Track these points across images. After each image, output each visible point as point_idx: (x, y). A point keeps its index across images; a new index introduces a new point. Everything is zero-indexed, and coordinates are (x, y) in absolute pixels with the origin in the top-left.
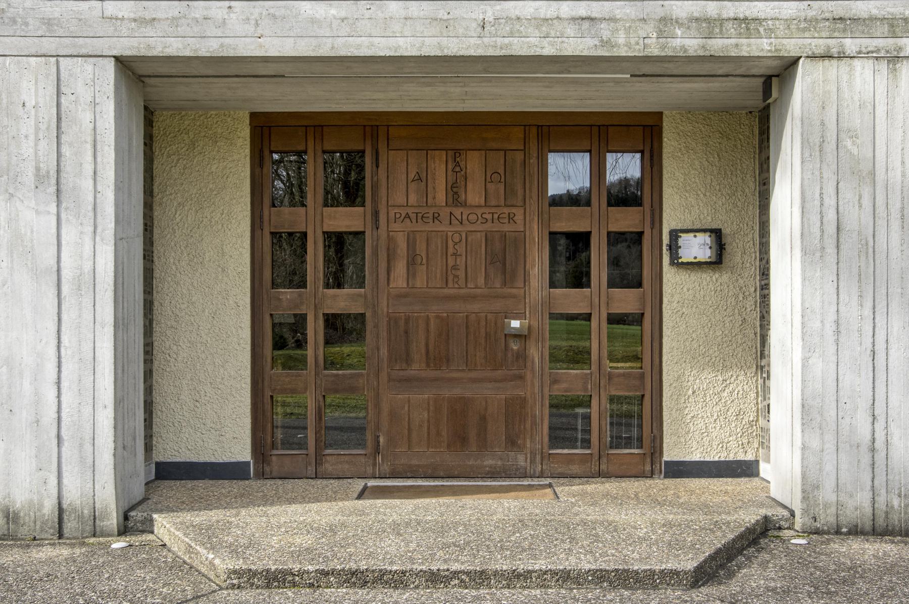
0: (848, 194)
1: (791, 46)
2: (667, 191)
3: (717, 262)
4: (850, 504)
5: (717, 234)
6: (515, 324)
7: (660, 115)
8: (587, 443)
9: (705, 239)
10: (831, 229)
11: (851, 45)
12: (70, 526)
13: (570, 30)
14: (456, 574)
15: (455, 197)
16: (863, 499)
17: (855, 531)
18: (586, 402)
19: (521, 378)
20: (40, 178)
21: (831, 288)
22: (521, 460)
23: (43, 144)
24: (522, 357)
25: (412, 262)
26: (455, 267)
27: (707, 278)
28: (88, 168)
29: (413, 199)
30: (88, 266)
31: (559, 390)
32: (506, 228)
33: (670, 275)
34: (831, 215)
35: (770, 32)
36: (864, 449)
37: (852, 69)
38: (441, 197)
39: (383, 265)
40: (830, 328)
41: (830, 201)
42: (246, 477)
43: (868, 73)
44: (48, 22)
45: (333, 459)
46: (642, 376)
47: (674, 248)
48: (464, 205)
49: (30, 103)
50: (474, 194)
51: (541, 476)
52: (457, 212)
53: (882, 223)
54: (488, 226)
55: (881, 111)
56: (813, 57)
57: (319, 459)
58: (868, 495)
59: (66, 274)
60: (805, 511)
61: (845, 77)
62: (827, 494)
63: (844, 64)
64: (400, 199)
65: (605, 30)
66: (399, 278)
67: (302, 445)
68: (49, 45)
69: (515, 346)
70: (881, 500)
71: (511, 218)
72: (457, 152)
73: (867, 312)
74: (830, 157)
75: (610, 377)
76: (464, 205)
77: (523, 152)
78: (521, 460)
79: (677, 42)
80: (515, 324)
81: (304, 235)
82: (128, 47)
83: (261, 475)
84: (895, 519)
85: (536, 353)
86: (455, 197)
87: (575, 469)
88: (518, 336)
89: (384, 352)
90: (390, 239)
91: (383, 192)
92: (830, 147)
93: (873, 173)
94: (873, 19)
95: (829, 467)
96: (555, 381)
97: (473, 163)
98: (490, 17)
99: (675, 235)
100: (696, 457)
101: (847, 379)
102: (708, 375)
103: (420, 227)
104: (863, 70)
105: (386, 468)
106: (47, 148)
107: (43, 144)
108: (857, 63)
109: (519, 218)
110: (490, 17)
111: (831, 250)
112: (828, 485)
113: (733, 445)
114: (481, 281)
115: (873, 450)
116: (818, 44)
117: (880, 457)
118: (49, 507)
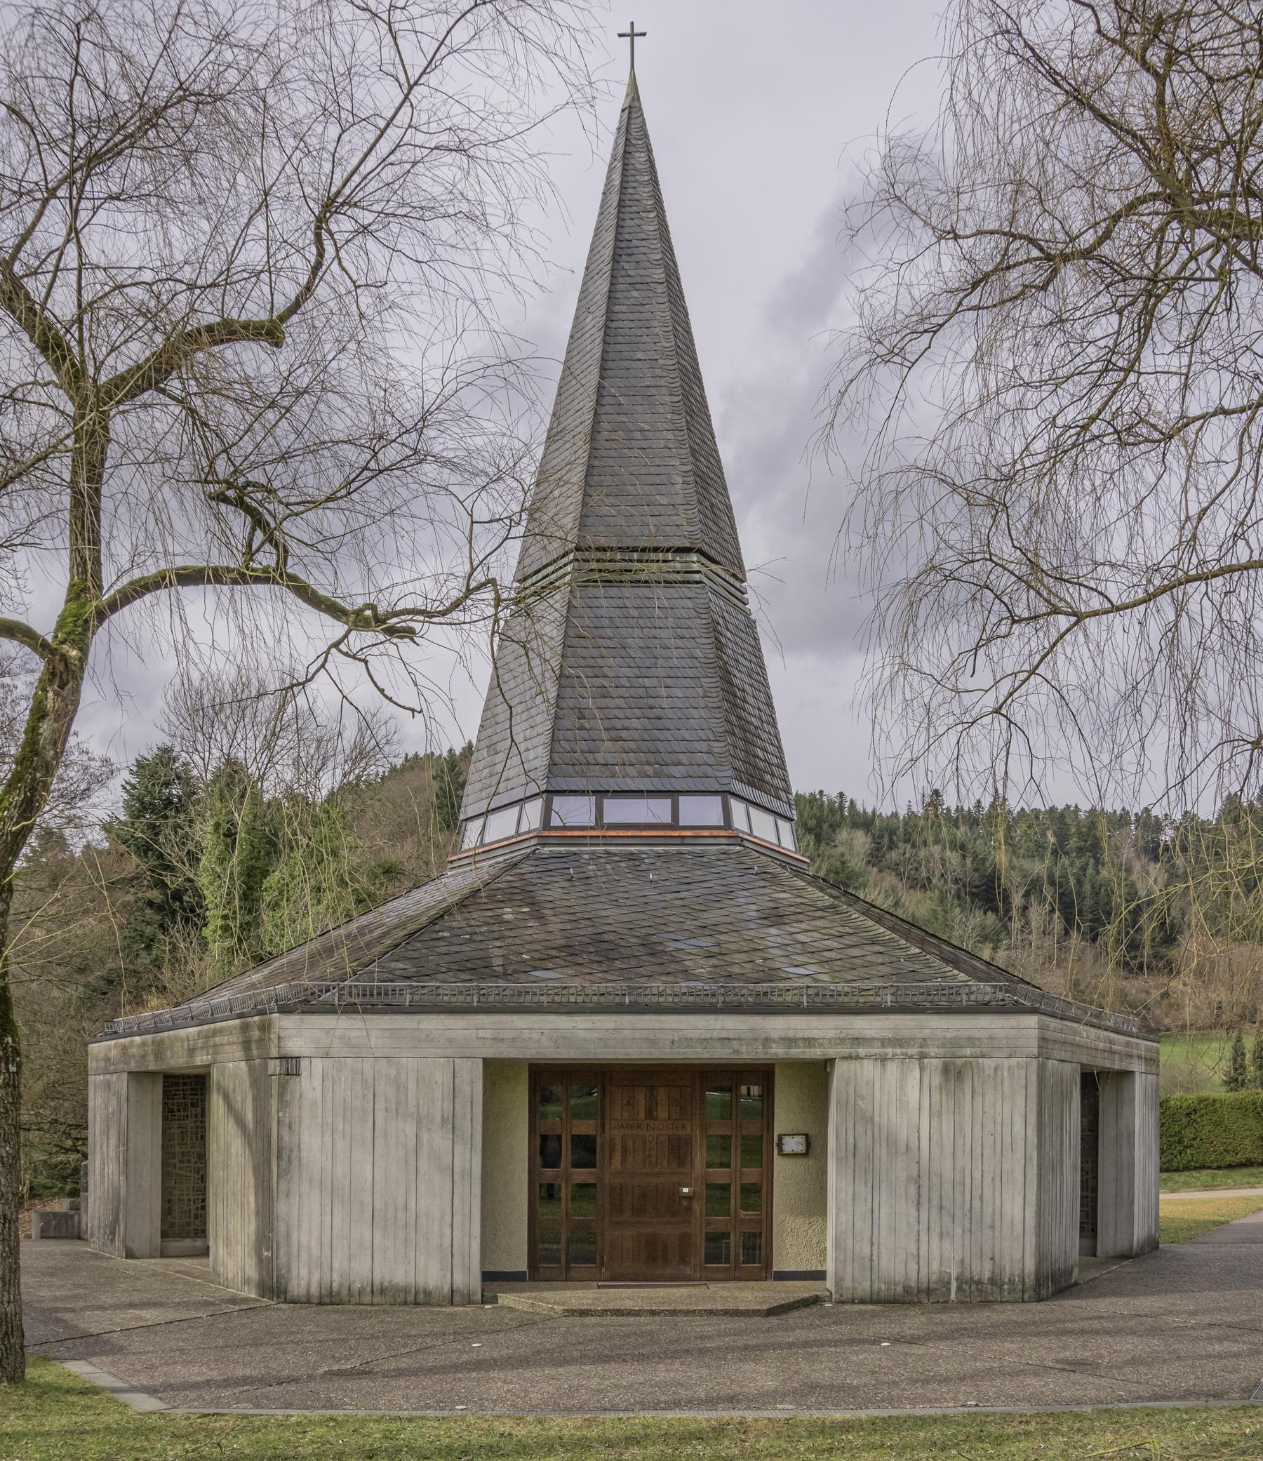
0: (859, 1128)
1: (831, 1052)
2: (777, 1111)
3: (806, 1155)
4: (860, 1288)
5: (807, 1135)
6: (686, 1190)
7: (773, 1065)
8: (727, 1261)
9: (801, 1139)
10: (851, 1147)
11: (862, 1052)
12: (457, 1298)
13: (718, 1045)
14: (662, 1311)
15: (650, 1114)
16: (866, 1285)
17: (862, 1302)
18: (726, 1235)
19: (689, 1222)
20: (444, 1120)
21: (850, 1178)
22: (688, 1271)
23: (446, 1103)
24: (689, 1209)
25: (625, 1151)
26: (650, 1156)
27: (800, 1164)
28: (468, 1116)
29: (626, 1115)
30: (467, 1166)
31: (204, 1261)
32: (680, 1133)
33: (778, 1161)
34: (851, 1140)
35: (821, 1045)
36: (867, 1260)
37: (862, 1065)
38: (642, 1115)
39: (607, 1154)
40: (850, 1198)
41: (851, 1133)
42: (524, 1280)
43: (871, 1066)
44: (450, 1040)
45: (577, 1269)
46: (761, 1221)
47: (780, 1145)
48: (656, 1119)
49: (440, 1082)
50: (662, 1113)
51: (700, 1280)
52: (652, 1123)
53: (877, 1144)
54: (670, 1132)
55: (877, 1086)
56: (843, 1058)
57: (568, 1269)
58: (868, 1283)
59: (456, 1169)
60: (837, 1292)
61: (859, 1069)
62: (848, 1283)
63: (858, 1063)
64: (617, 1115)
65: (736, 1045)
66: (617, 1163)
67: (559, 1261)
68: (450, 1052)
69: (685, 1203)
70: (875, 1286)
71: (683, 1127)
72: (652, 1088)
73: (869, 1189)
74: (851, 1110)
75: (742, 1220)
76: (656, 1119)
77: (682, 799)
78: (688, 1271)
79: (773, 1051)
80: (686, 1190)
81: (559, 1137)
82: (490, 1053)
83: (533, 1279)
84: (882, 1295)
85: (698, 1207)
86: (650, 1114)
87: (721, 1275)
88: (688, 1197)
89: (607, 1206)
90: (611, 1140)
91: (607, 1113)
92: (851, 1105)
93: (872, 1119)
94: (873, 1039)
95: (849, 1269)
96: (709, 1223)
97: (662, 1094)
98: (676, 1038)
99: (780, 1137)
100: (793, 1268)
101: (858, 1225)
102: (800, 1220)
103: (629, 1132)
104: (868, 1066)
105: (608, 1275)
106: (448, 1105)
107: (446, 1103)
108: (865, 1062)
109: (689, 1127)
110: (676, 1038)
111: (851, 1158)
112: (848, 1278)
113: (814, 1261)
114: (665, 1163)
115: (871, 1260)
116: (845, 1051)
117: (875, 1263)
118: (446, 1289)
